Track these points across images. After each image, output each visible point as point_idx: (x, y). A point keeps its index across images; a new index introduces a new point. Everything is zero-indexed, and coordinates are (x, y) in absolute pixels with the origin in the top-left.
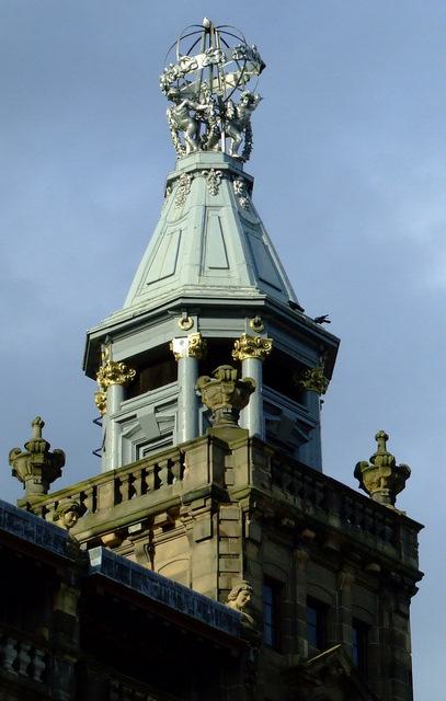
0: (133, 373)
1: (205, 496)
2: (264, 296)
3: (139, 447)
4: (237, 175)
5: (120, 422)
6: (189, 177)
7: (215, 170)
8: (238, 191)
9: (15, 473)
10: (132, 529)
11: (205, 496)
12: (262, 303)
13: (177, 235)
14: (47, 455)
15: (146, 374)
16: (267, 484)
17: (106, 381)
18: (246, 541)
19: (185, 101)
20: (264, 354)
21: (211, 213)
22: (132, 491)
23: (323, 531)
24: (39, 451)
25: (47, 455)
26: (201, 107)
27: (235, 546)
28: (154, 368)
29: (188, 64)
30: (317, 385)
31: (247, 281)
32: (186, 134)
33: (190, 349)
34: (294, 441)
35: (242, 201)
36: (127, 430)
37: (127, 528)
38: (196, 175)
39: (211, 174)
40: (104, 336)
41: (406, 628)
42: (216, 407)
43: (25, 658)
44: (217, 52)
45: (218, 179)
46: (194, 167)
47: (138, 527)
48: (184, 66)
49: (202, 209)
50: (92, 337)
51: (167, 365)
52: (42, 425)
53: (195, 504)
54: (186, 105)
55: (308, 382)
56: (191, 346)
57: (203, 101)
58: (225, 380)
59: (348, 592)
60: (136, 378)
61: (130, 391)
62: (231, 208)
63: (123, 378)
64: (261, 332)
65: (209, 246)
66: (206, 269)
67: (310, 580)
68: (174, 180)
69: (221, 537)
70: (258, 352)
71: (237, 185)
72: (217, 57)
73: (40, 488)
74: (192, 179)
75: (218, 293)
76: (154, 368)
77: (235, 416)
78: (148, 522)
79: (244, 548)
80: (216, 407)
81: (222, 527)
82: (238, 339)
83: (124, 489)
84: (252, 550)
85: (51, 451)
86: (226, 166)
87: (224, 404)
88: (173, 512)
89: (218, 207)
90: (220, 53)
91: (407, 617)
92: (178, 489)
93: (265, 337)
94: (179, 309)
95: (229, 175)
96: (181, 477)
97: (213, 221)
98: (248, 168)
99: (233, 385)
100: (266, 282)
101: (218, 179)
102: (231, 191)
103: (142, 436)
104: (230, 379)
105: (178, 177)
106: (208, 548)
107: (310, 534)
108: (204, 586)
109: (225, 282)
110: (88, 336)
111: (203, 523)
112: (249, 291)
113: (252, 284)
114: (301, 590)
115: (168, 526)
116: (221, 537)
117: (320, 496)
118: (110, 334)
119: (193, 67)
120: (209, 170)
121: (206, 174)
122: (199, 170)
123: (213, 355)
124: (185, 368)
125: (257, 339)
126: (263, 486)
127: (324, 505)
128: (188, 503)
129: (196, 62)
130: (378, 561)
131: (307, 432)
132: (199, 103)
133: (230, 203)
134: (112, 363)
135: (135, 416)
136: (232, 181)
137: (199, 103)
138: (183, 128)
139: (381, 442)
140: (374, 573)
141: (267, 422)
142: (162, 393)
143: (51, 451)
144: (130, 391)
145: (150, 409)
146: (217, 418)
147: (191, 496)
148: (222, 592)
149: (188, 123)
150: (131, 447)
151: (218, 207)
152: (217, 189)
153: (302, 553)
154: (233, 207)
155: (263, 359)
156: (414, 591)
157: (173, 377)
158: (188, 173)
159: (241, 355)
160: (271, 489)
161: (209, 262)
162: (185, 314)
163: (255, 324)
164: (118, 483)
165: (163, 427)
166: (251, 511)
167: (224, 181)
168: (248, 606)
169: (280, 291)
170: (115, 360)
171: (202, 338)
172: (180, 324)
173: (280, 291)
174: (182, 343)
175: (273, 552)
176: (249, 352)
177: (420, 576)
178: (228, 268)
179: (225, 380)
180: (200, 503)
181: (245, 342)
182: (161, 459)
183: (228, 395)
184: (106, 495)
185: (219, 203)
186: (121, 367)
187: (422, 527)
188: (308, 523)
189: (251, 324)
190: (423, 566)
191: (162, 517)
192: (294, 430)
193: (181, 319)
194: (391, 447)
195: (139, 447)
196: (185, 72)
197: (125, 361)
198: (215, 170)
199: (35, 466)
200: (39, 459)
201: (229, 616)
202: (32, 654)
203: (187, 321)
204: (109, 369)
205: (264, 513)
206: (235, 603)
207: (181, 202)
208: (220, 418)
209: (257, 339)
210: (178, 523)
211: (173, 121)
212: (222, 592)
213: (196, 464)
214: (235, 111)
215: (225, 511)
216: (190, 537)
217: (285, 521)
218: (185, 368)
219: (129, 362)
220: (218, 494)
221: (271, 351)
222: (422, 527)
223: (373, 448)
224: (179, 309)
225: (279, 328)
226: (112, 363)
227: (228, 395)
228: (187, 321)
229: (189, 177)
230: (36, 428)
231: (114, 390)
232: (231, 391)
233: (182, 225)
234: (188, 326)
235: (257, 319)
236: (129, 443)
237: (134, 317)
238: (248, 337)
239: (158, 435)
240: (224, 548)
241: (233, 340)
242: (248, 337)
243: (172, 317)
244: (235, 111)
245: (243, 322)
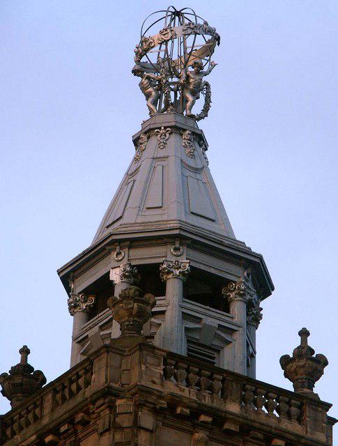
16: (157, 381)
22: (64, 399)
37: (273, 439)
45: (168, 135)
55: (234, 293)
78: (70, 420)
81: (118, 420)
100: (198, 215)
101: (168, 135)
115: (85, 423)
118: (195, 241)
120: (160, 128)
126: (154, 382)
128: (93, 403)
135: (87, 337)
141: (187, 329)
142: (189, 306)
145: (96, 328)
147: (95, 397)
160: (162, 385)
169: (213, 221)
173: (213, 221)
182: (80, 369)
185: (165, 155)
187: (330, 406)
188: (197, 411)
194: (311, 342)
198: (165, 128)
203: (121, 253)
213: (99, 369)
217: (179, 410)
223: (17, 360)
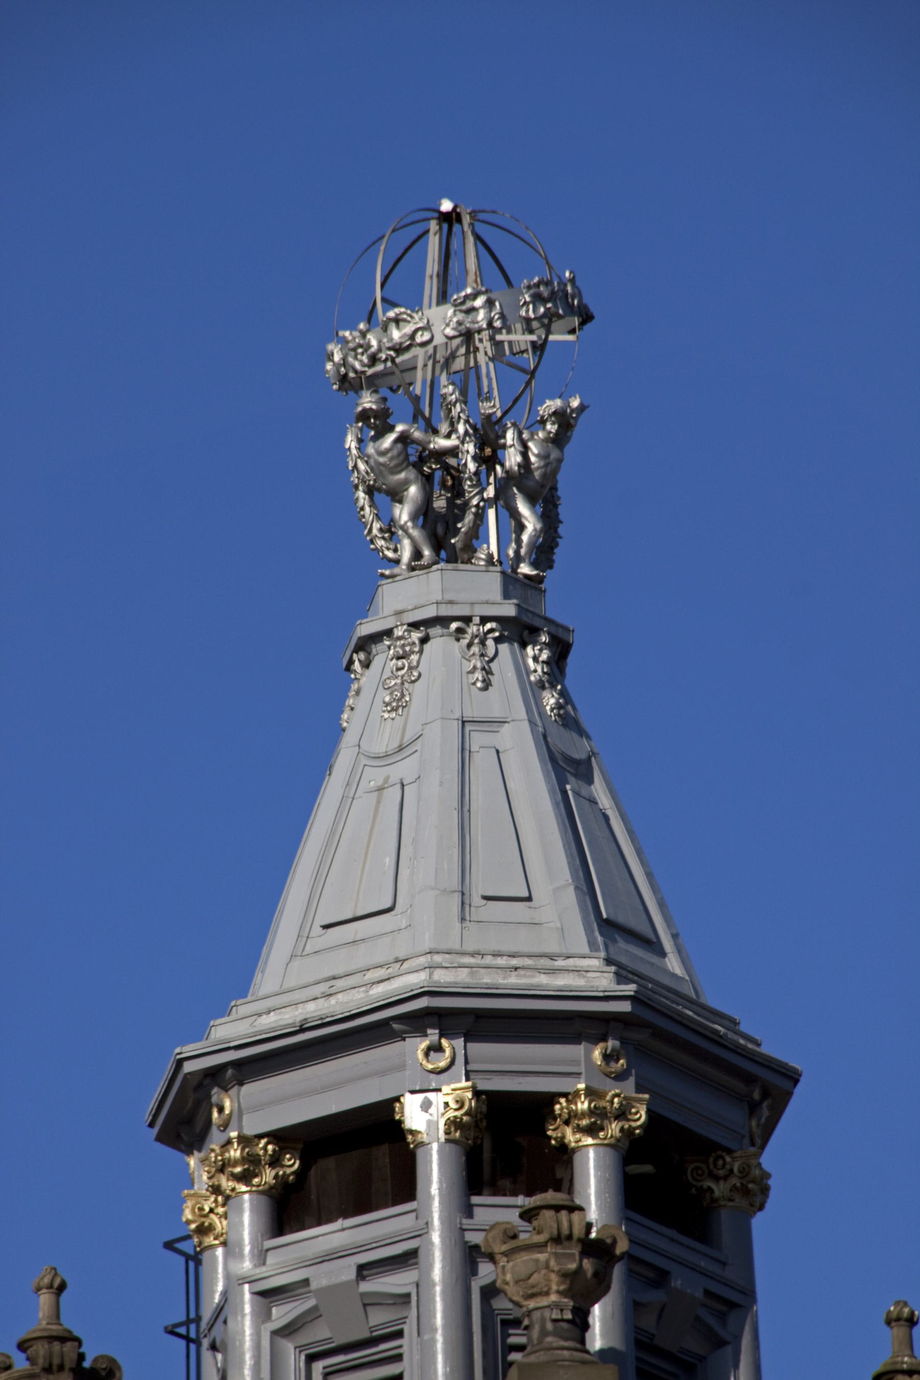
0: (291, 1164)
2: (630, 989)
3: (312, 1358)
4: (535, 631)
5: (263, 1294)
6: (416, 636)
7: (484, 620)
8: (537, 670)
12: (625, 1007)
13: (394, 794)
17: (226, 1184)
19: (400, 428)
20: (627, 1133)
24: (61, 1368)
26: (442, 443)
29: (408, 329)
30: (745, 1192)
31: (578, 939)
32: (403, 514)
33: (449, 1123)
34: (693, 1344)
35: (550, 700)
36: (282, 1314)
38: (435, 631)
39: (473, 629)
40: (222, 1068)
42: (532, 1304)
44: (479, 302)
45: (490, 643)
46: (430, 612)
49: (456, 726)
50: (189, 1067)
52: (62, 1287)
54: (403, 439)
56: (451, 1114)
57: (444, 428)
58: (557, 1239)
60: (301, 1174)
62: (526, 725)
63: (268, 1176)
64: (620, 1077)
66: (477, 900)
68: (376, 637)
70: (614, 1129)
72: (481, 315)
74: (424, 640)
75: (514, 980)
80: (532, 1304)
82: (565, 1095)
85: (87, 1364)
86: (509, 610)
87: (554, 1298)
89: (493, 723)
90: (490, 303)
93: (628, 1087)
97: (482, 763)
99: (576, 1251)
101: (490, 643)
102: (522, 671)
104: (570, 1237)
105: (389, 633)
109: (523, 941)
110: (179, 1063)
113: (592, 945)
119: (419, 339)
120: (467, 620)
121: (460, 631)
122: (442, 621)
129: (427, 327)
131: (722, 1317)
132: (436, 432)
133: (523, 714)
134: (244, 1140)
136: (524, 645)
137: (436, 432)
139: (899, 1331)
143: (87, 1364)
145: (346, 1271)
146: (535, 1333)
149: (406, 484)
151: (493, 723)
152: (488, 672)
154: (532, 722)
155: (626, 1144)
158: (415, 625)
159: (571, 1137)
161: (480, 886)
162: (433, 1035)
163: (607, 1057)
165: (379, 1318)
167: (504, 648)
170: (249, 1131)
171: (477, 1093)
172: (420, 1055)
174: (426, 1106)
176: (591, 1130)
178: (529, 899)
179: (557, 1239)
181: (583, 1105)
183: (565, 1275)
189: (597, 1054)
190: (561, 517)
192: (698, 1319)
193: (425, 1044)
195: (312, 1358)
196: (399, 349)
197: (276, 1136)
198: (484, 620)
203: (439, 1049)
204: (235, 1153)
207: (398, 705)
208: (544, 1333)
211: (362, 466)
214: (525, 454)
221: (646, 1127)
226: (244, 1140)
227: (565, 1275)
228: (439, 1049)
229: (416, 636)
230: (45, 1299)
232: (573, 1266)
233: (405, 769)
234: (442, 1064)
235: (612, 1044)
236: (289, 1347)
237: (302, 1030)
238: (591, 1093)
239: (363, 1334)
241: (551, 1098)
242: (591, 1093)
243: (401, 1036)
244: (525, 454)
245: (576, 1051)
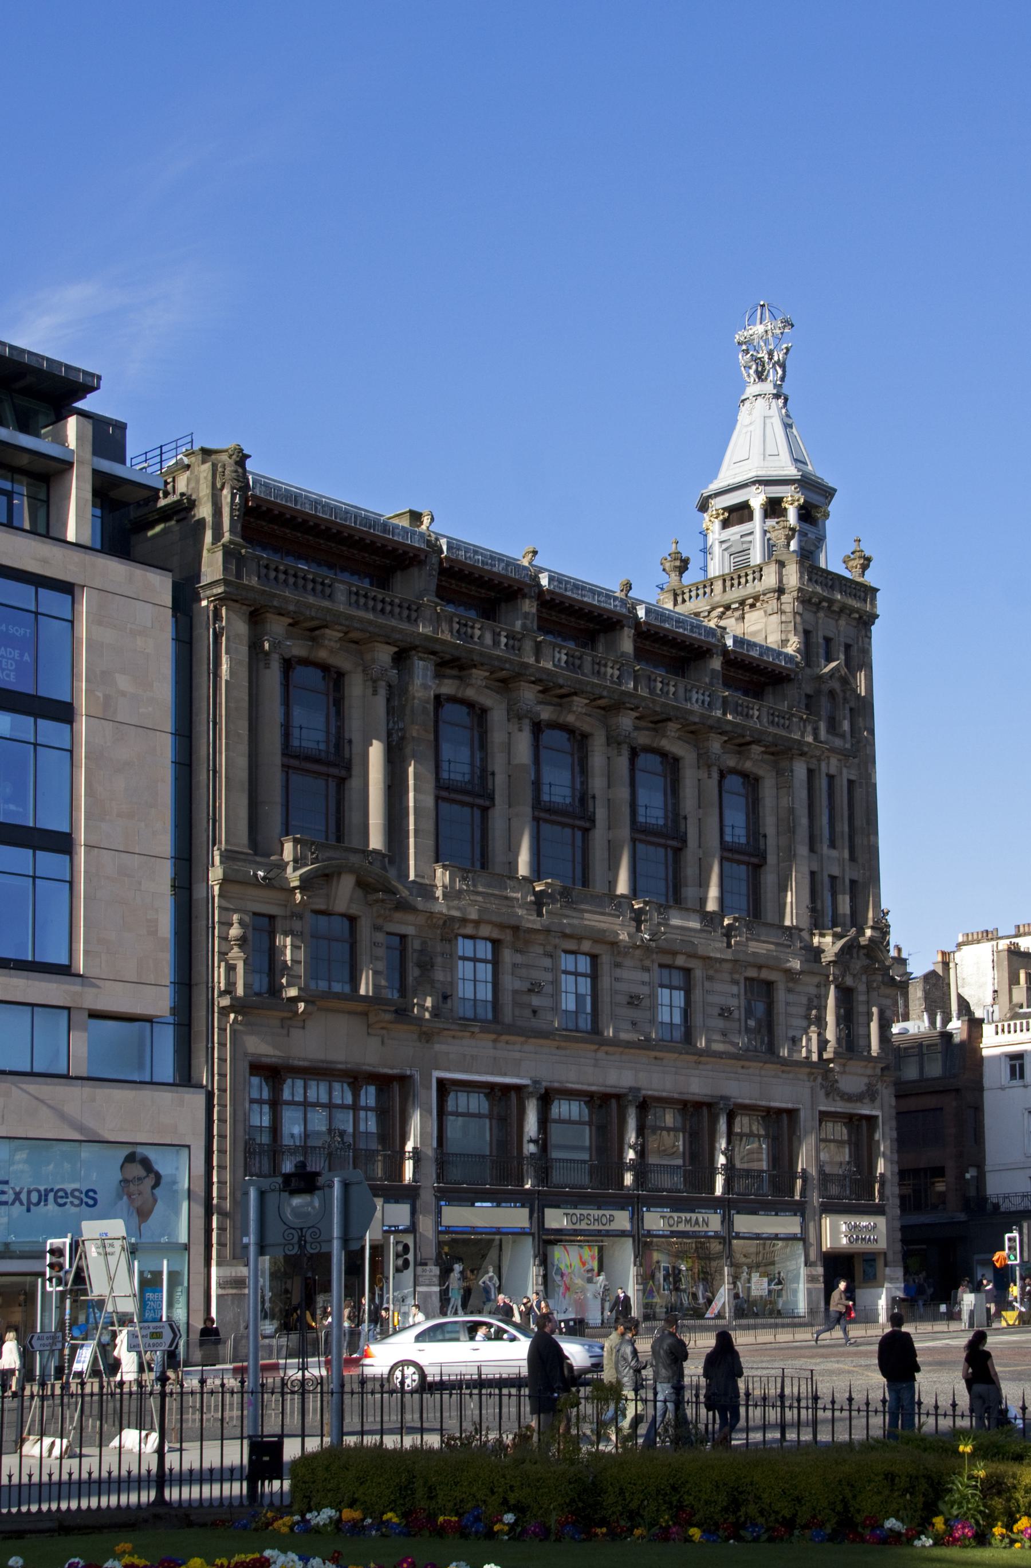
0: (726, 514)
1: (774, 591)
9: (664, 570)
10: (733, 606)
11: (774, 591)
14: (682, 561)
15: (735, 515)
18: (795, 613)
21: (768, 421)
23: (831, 602)
25: (682, 561)
27: (789, 617)
28: (739, 513)
34: (812, 548)
35: (784, 411)
36: (724, 546)
41: (870, 644)
43: (701, 697)
47: (737, 605)
48: (751, 332)
51: (746, 511)
53: (768, 596)
59: (843, 629)
61: (726, 524)
63: (721, 517)
65: (767, 439)
67: (826, 626)
69: (783, 612)
70: (796, 504)
71: (781, 402)
73: (678, 578)
76: (739, 513)
77: (788, 545)
78: (742, 603)
79: (794, 618)
83: (728, 583)
84: (798, 619)
88: (756, 598)
91: (870, 638)
92: (759, 587)
94: (754, 483)
95: (777, 396)
96: (761, 579)
97: (768, 426)
98: (785, 390)
102: (777, 405)
103: (733, 550)
106: (775, 619)
107: (825, 604)
108: (773, 640)
111: (773, 604)
112: (791, 471)
114: (821, 634)
116: (783, 612)
117: (830, 583)
123: (774, 508)
124: (758, 514)
125: (797, 496)
127: (832, 588)
128: (765, 594)
130: (857, 612)
138: (750, 368)
140: (855, 619)
144: (726, 524)
148: (785, 642)
150: (727, 555)
153: (821, 614)
156: (873, 623)
157: (750, 518)
159: (787, 506)
161: (768, 452)
164: (724, 581)
165: (745, 546)
166: (798, 598)
168: (798, 651)
175: (809, 616)
177: (877, 616)
180: (772, 595)
184: (718, 586)
186: (721, 511)
187: (877, 590)
188: (824, 599)
191: (750, 601)
194: (863, 546)
197: (723, 509)
199: (676, 567)
200: (678, 563)
201: (789, 658)
202: (703, 694)
205: (805, 599)
206: (790, 650)
209: (797, 496)
210: (758, 604)
212: (785, 642)
213: (769, 574)
215: (785, 598)
216: (765, 612)
218: (758, 514)
219: (725, 509)
220: (780, 591)
222: (877, 590)
224: (754, 483)
225: (809, 490)
230: (674, 545)
231: (717, 525)
233: (751, 428)
240: (784, 618)
